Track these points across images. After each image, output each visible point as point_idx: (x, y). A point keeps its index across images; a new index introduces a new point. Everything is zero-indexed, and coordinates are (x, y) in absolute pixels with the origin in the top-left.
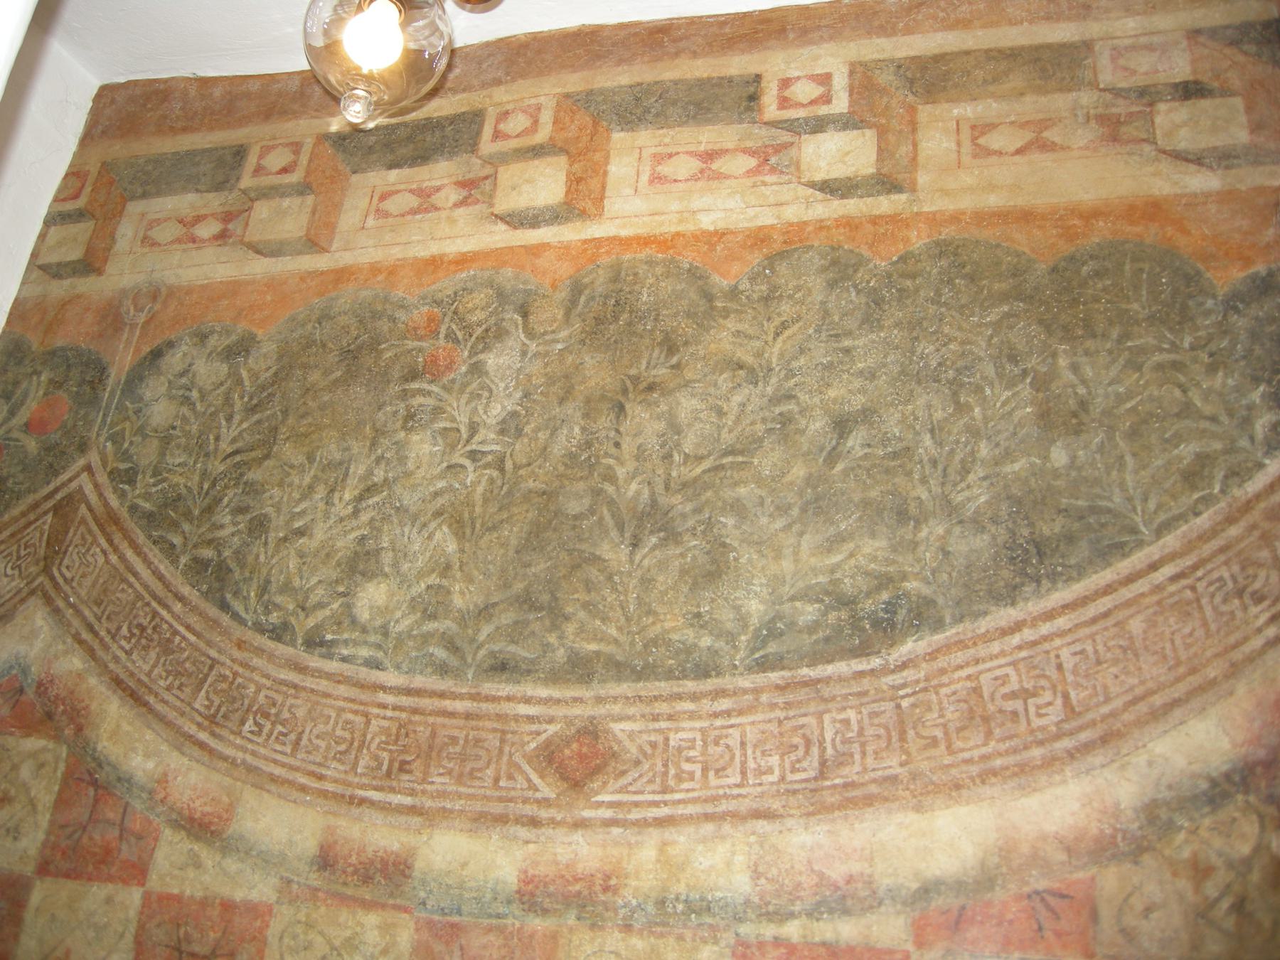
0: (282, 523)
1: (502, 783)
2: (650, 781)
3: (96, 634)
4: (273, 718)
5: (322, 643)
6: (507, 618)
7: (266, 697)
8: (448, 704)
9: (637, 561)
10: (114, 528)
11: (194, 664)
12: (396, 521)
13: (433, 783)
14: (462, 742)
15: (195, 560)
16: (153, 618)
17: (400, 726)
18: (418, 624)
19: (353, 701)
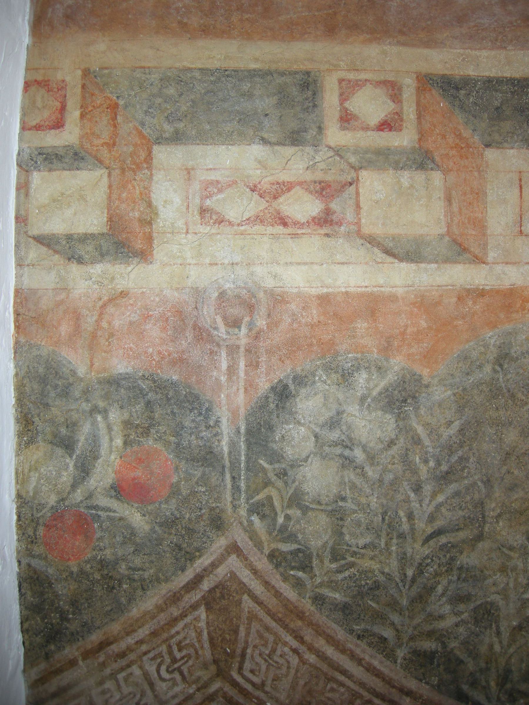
10: (300, 623)
15: (415, 652)
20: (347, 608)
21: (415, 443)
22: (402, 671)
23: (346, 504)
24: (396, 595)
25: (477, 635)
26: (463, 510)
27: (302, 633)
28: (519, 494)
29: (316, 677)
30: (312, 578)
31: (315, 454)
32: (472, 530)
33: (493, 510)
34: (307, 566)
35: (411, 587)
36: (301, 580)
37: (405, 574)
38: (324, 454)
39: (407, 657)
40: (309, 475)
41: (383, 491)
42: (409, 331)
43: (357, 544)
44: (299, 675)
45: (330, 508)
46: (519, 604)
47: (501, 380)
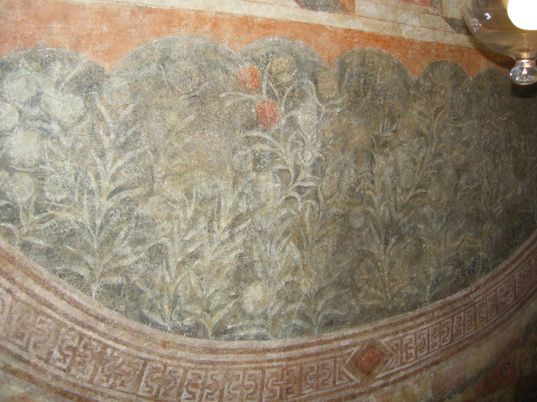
0: (177, 250)
1: (337, 383)
2: (397, 362)
3: (28, 362)
4: (201, 386)
5: (225, 332)
6: (331, 295)
7: (193, 374)
8: (306, 350)
9: (387, 253)
10: (11, 267)
11: (129, 365)
12: (260, 241)
13: (304, 394)
14: (316, 368)
15: (106, 286)
16: (81, 339)
17: (283, 370)
18: (284, 307)
19: (251, 362)
20: (50, 252)
21: (100, 120)
22: (97, 302)
23: (46, 167)
24: (88, 240)
25: (152, 270)
26: (137, 172)
27: (13, 276)
28: (178, 161)
29: (28, 312)
30: (19, 229)
31: (19, 126)
32: (144, 187)
33: (160, 173)
34: (15, 219)
35: (100, 233)
36: (11, 231)
37: (95, 223)
38: (27, 126)
39: (100, 290)
40: (14, 143)
41: (75, 157)
42: (94, 33)
43: (56, 199)
44: (13, 311)
45: (32, 170)
46: (182, 244)
47: (163, 75)
